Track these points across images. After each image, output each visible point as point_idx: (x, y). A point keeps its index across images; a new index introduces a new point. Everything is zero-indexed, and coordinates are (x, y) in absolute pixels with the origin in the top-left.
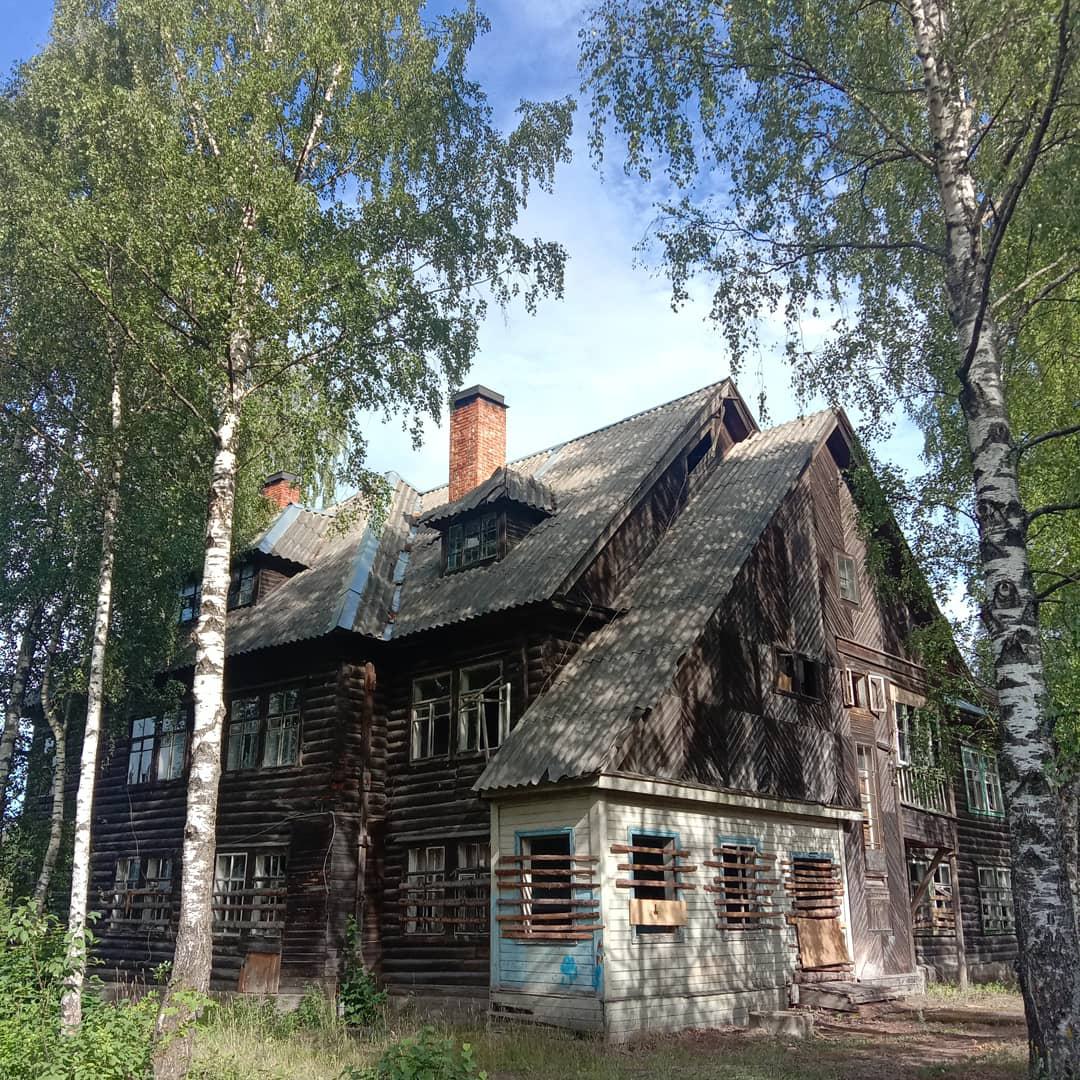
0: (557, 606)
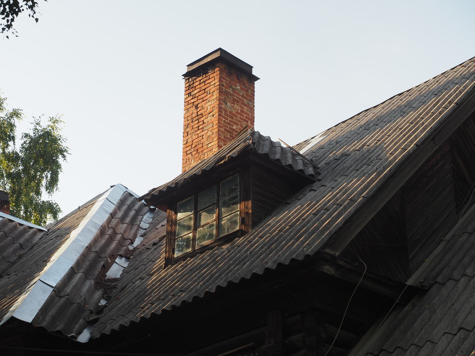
0: (328, 269)
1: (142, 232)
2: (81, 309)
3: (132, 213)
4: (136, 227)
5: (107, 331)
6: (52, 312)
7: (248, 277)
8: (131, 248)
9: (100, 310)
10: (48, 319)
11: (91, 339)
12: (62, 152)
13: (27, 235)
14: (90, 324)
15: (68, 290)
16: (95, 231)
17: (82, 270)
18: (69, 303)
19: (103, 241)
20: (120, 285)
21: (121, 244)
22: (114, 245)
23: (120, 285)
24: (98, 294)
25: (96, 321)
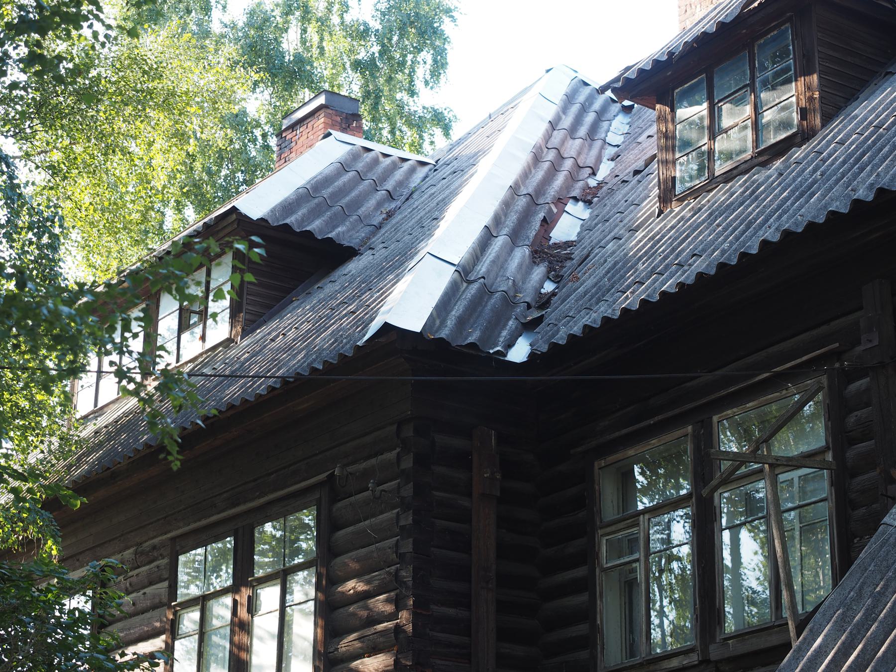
1: (610, 151)
2: (509, 302)
3: (590, 118)
4: (598, 144)
5: (561, 338)
6: (457, 311)
7: (821, 219)
8: (592, 183)
9: (544, 302)
10: (450, 322)
11: (532, 356)
12: (448, 11)
13: (399, 175)
14: (529, 327)
15: (482, 268)
16: (524, 158)
17: (505, 231)
18: (486, 292)
19: (539, 175)
20: (578, 254)
21: (573, 178)
22: (560, 180)
23: (578, 254)
24: (539, 271)
25: (538, 321)
